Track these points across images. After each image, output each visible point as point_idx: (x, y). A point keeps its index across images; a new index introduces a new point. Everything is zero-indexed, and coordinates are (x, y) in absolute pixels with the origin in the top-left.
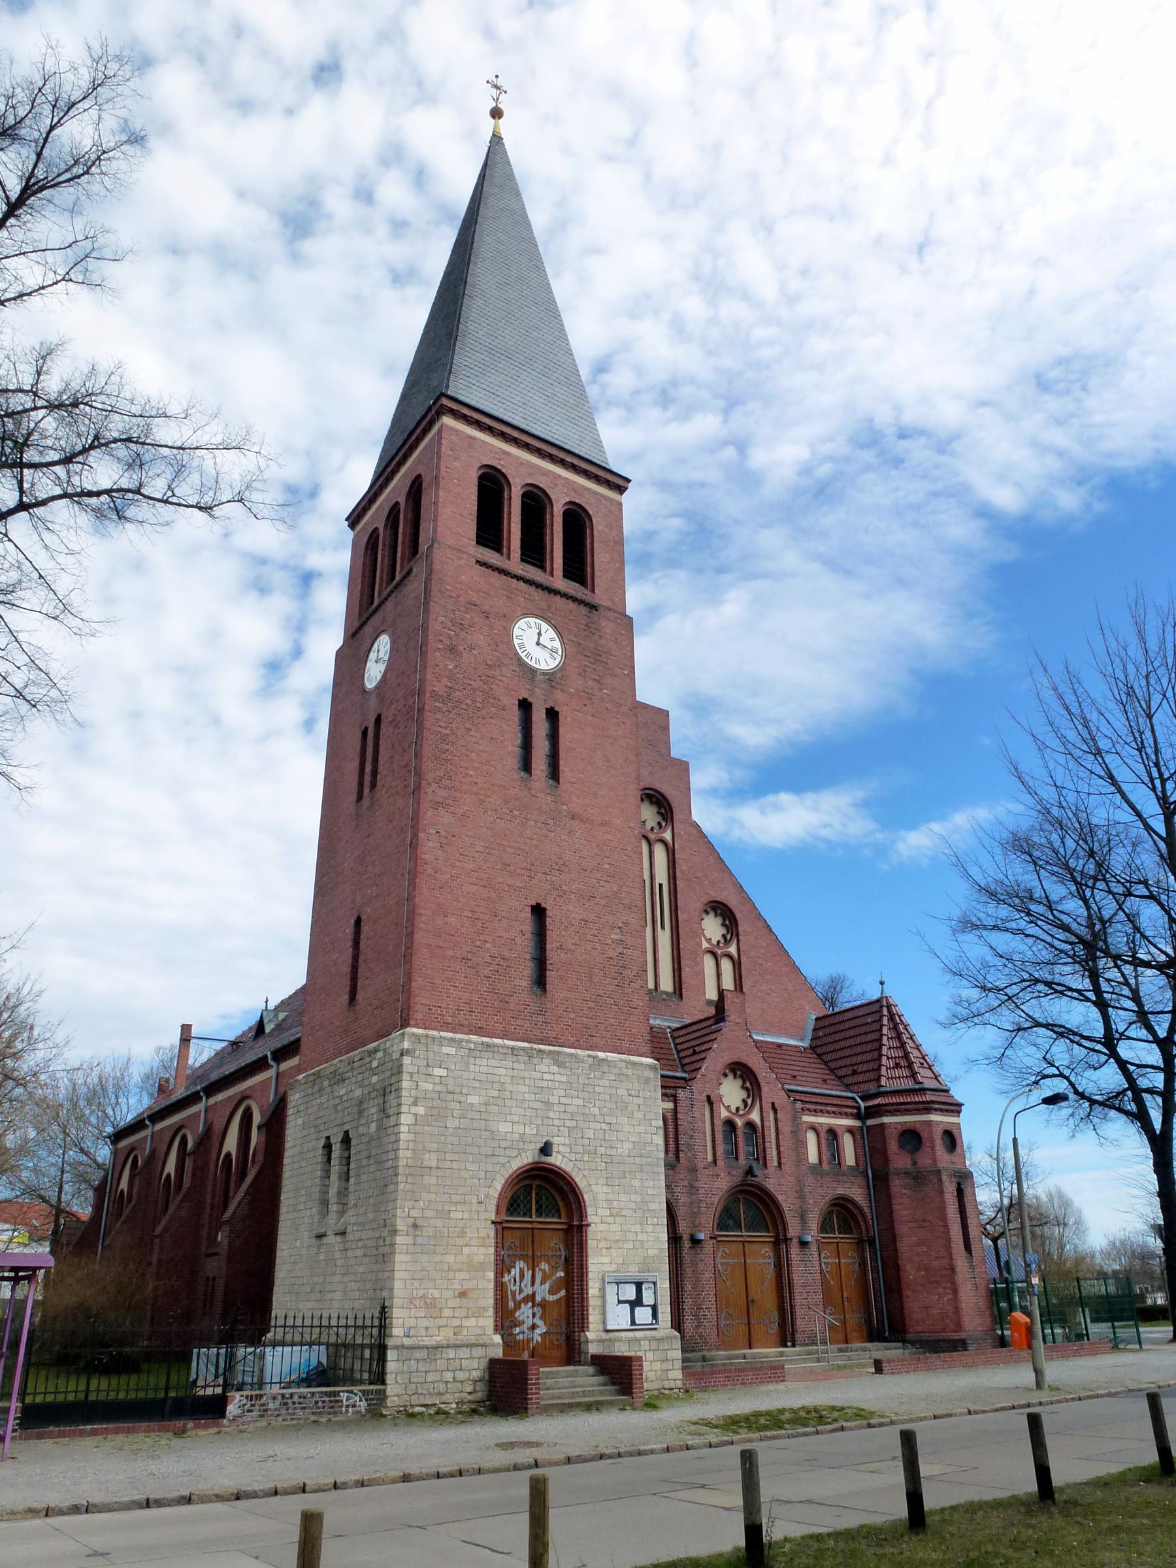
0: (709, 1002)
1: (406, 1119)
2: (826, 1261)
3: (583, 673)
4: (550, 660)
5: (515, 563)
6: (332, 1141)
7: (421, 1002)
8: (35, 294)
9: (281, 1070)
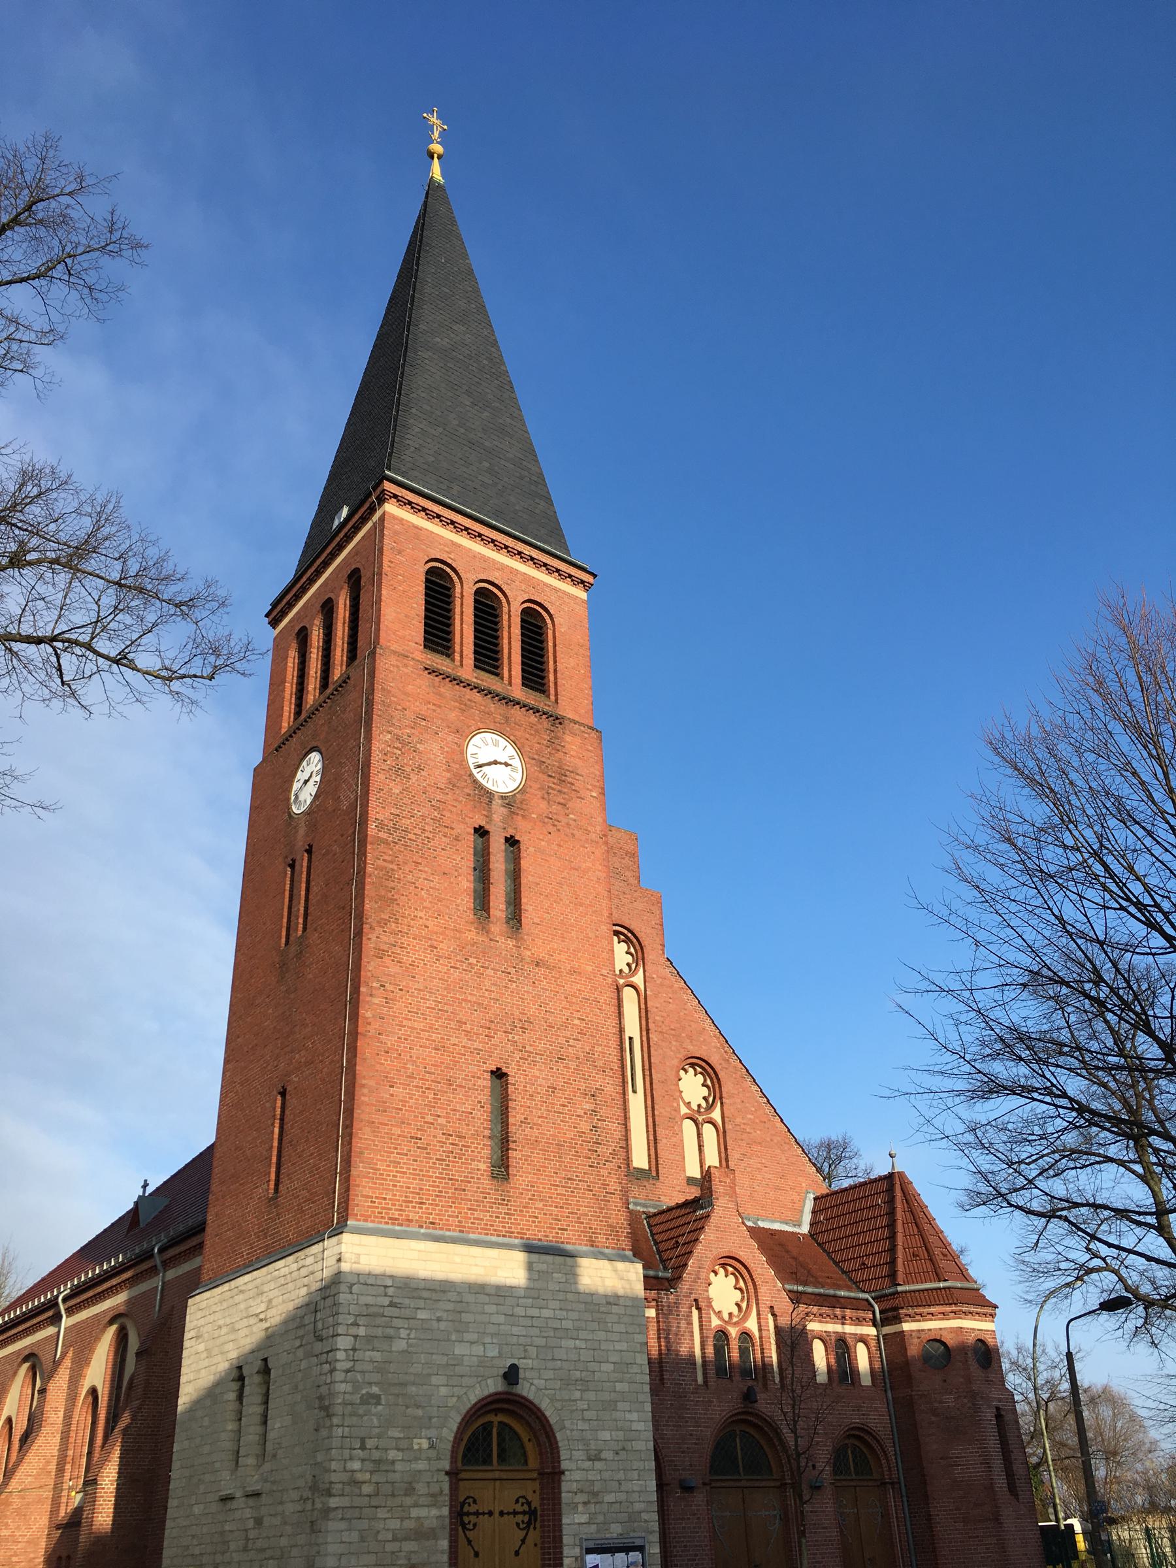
0: (691, 1181)
1: (343, 1343)
3: (546, 796)
5: (468, 671)
6: (245, 1372)
7: (364, 1190)
9: (166, 1280)
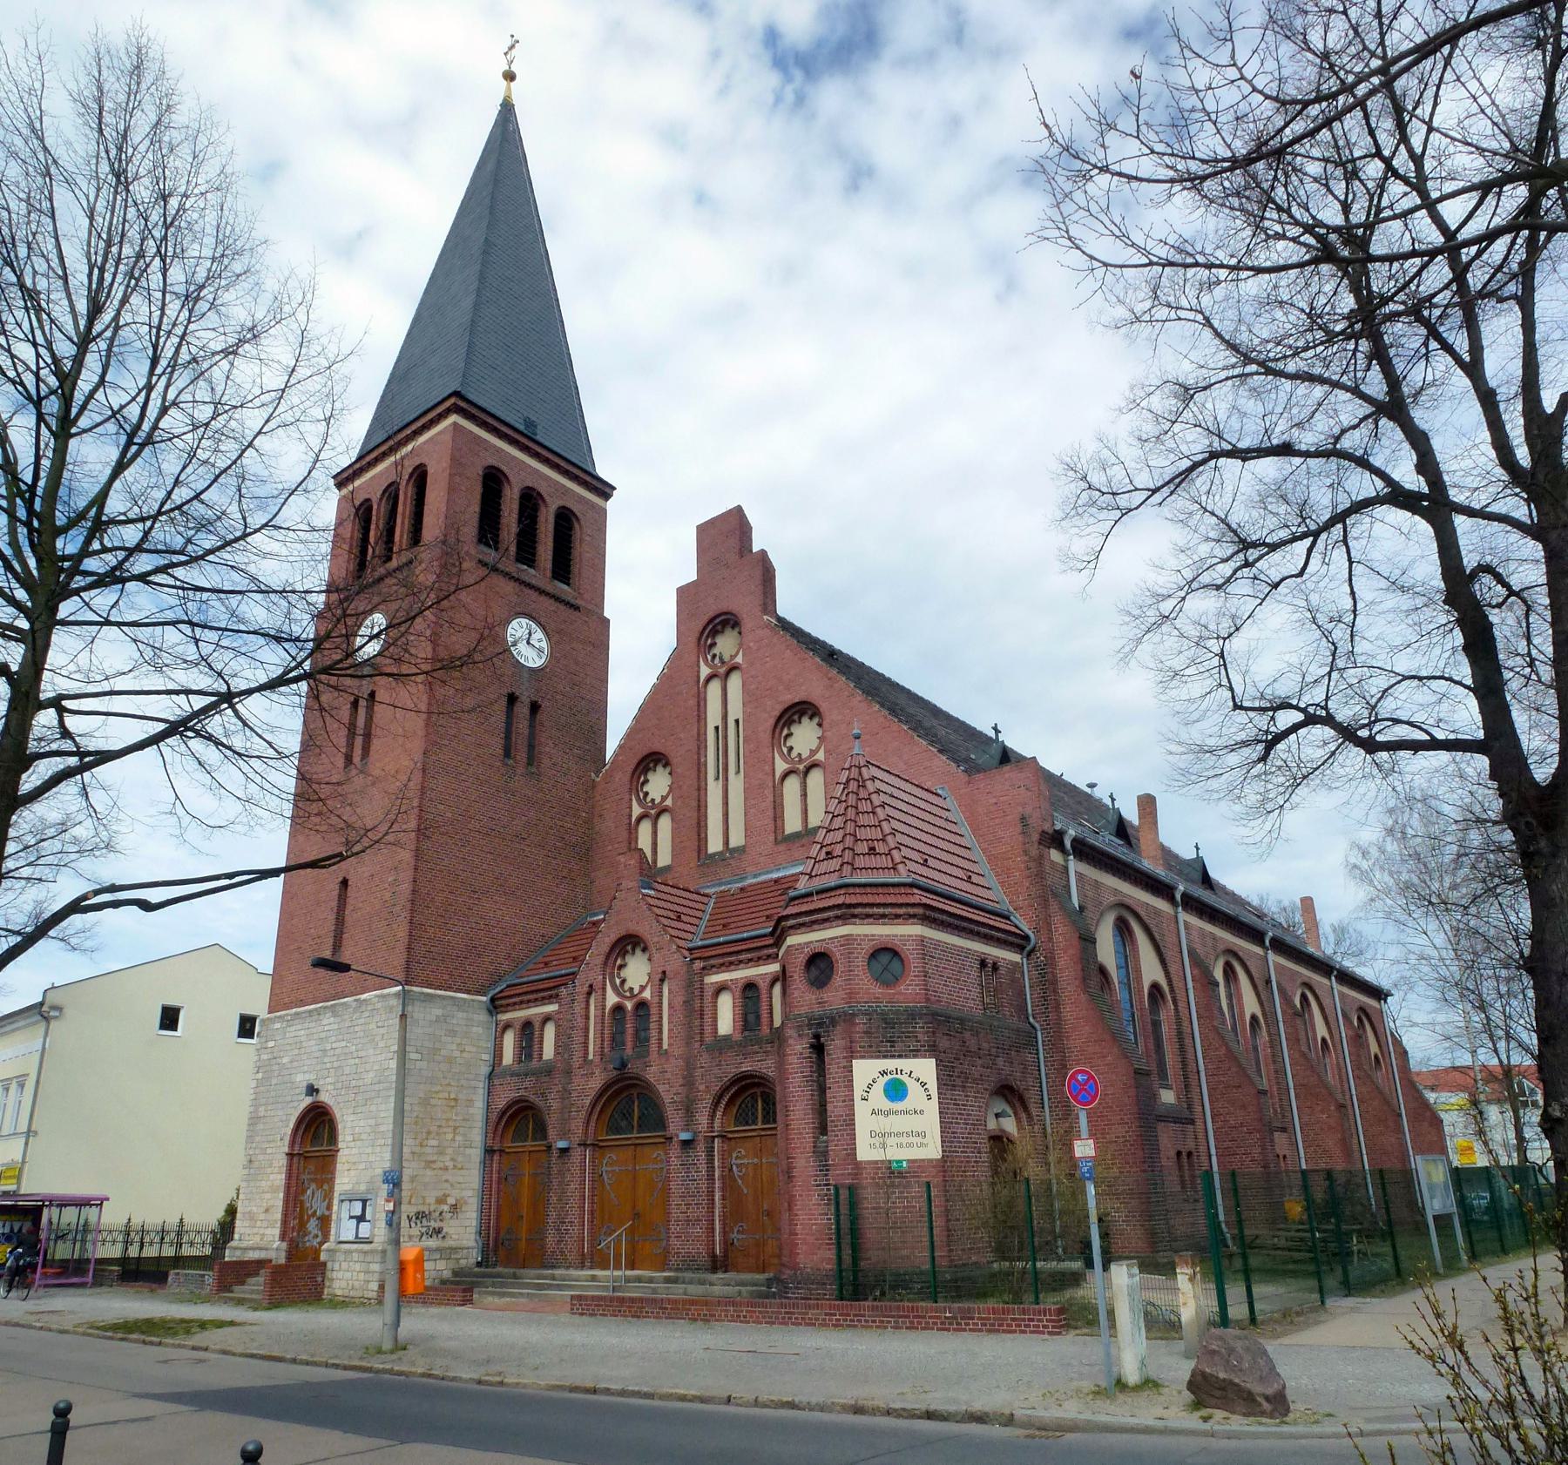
2: (739, 1162)
4: (537, 659)
8: (1199, 458)
